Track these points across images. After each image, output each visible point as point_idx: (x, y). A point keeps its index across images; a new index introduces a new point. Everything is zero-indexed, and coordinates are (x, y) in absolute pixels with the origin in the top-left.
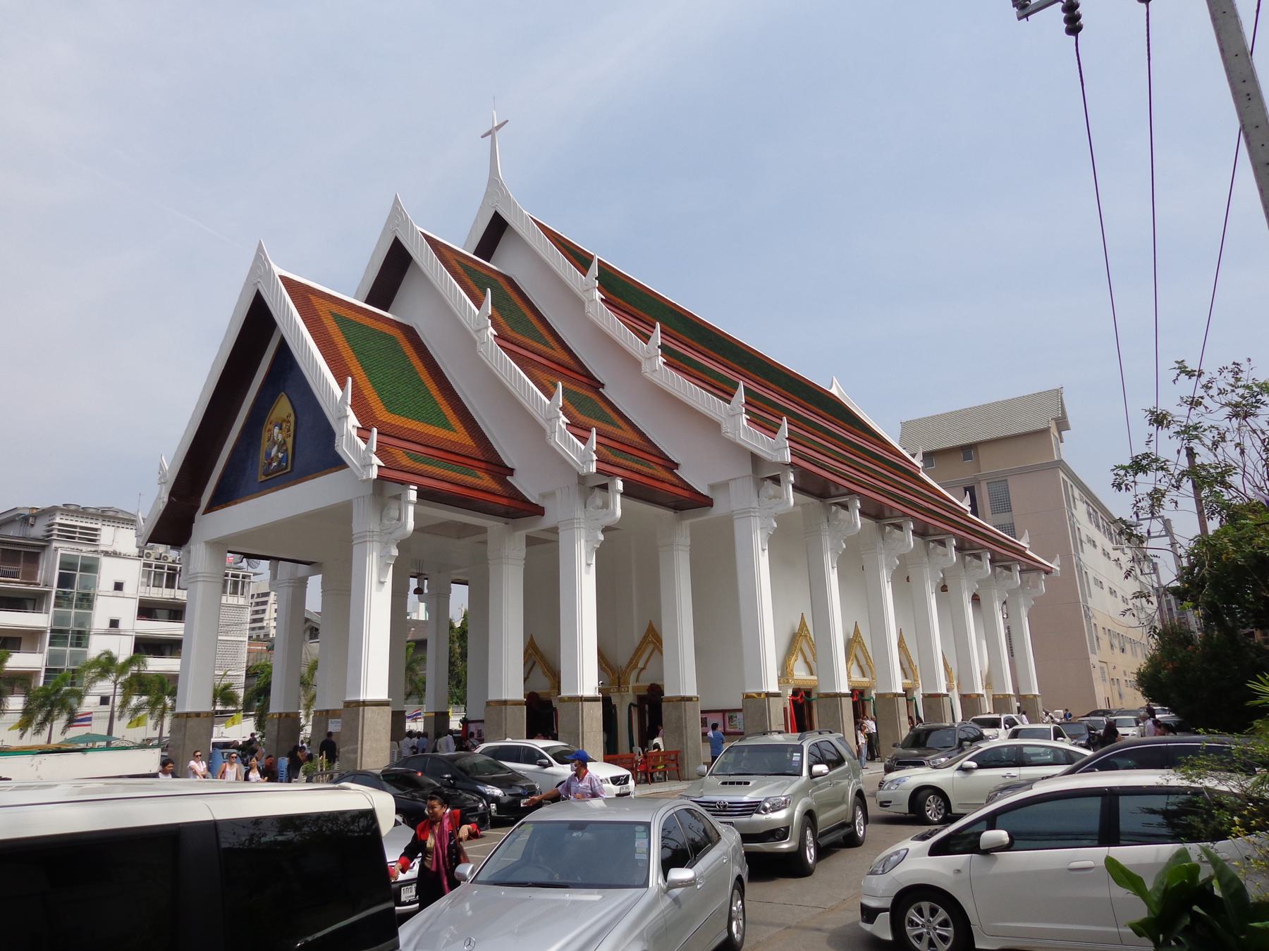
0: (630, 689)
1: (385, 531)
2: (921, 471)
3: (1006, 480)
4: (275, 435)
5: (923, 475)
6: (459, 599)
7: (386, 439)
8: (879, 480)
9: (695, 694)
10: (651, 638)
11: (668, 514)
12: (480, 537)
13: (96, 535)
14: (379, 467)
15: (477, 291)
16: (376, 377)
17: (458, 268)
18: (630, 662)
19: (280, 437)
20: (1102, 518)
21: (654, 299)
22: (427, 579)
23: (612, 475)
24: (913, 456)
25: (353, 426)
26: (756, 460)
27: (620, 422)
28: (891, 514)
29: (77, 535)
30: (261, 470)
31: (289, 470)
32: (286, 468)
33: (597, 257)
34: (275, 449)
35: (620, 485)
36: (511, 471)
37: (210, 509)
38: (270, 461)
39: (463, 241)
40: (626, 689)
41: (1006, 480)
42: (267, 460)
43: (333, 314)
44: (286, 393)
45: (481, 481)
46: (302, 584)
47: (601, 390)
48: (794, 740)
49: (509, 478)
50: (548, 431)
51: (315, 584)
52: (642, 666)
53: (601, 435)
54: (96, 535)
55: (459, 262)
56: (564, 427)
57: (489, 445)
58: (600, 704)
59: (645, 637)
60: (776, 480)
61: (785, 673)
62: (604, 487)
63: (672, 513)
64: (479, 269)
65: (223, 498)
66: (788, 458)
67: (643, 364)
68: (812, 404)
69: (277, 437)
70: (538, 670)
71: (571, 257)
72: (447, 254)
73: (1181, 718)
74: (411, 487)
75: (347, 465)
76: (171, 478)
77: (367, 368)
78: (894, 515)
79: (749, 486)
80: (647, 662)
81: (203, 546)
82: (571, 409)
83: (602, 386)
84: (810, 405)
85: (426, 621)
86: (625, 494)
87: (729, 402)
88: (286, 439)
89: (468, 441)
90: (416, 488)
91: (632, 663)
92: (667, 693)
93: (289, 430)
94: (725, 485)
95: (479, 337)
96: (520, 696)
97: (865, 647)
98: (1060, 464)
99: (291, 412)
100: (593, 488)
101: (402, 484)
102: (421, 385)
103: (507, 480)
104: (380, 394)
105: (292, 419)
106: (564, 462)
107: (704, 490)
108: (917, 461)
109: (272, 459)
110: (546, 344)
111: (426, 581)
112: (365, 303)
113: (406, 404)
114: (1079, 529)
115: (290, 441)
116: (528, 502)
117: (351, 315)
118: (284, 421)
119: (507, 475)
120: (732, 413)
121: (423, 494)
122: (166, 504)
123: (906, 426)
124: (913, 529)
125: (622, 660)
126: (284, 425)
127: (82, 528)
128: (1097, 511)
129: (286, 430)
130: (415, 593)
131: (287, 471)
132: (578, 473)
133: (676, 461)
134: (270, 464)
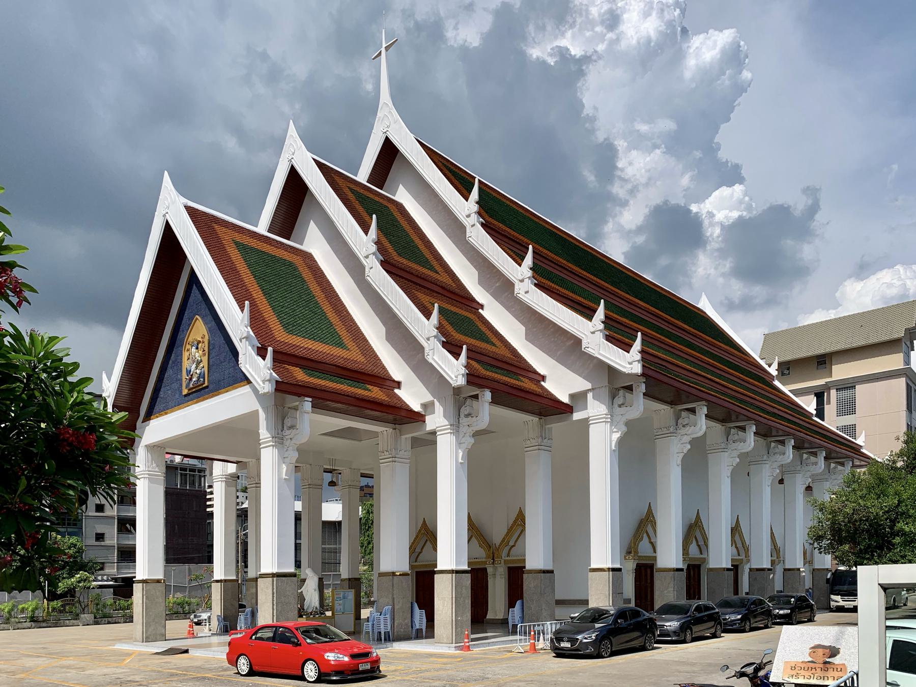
0: (502, 562)
5: (777, 383)
15: (364, 215)
16: (276, 300)
17: (351, 196)
21: (536, 223)
24: (770, 366)
26: (612, 372)
27: (498, 343)
33: (477, 178)
34: (194, 366)
42: (188, 376)
43: (236, 243)
45: (370, 392)
50: (427, 350)
52: (513, 544)
53: (472, 351)
55: (351, 189)
57: (378, 361)
58: (469, 575)
60: (629, 388)
64: (371, 196)
67: (516, 287)
68: (678, 320)
71: (456, 182)
72: (340, 182)
73: (701, 296)
74: (307, 399)
77: (267, 293)
82: (449, 328)
84: (677, 322)
85: (343, 504)
90: (310, 399)
91: (505, 541)
95: (367, 263)
96: (405, 567)
100: (466, 399)
103: (395, 394)
104: (279, 317)
107: (565, 399)
108: (773, 371)
110: (432, 268)
117: (253, 243)
124: (793, 444)
131: (204, 386)
134: (191, 379)
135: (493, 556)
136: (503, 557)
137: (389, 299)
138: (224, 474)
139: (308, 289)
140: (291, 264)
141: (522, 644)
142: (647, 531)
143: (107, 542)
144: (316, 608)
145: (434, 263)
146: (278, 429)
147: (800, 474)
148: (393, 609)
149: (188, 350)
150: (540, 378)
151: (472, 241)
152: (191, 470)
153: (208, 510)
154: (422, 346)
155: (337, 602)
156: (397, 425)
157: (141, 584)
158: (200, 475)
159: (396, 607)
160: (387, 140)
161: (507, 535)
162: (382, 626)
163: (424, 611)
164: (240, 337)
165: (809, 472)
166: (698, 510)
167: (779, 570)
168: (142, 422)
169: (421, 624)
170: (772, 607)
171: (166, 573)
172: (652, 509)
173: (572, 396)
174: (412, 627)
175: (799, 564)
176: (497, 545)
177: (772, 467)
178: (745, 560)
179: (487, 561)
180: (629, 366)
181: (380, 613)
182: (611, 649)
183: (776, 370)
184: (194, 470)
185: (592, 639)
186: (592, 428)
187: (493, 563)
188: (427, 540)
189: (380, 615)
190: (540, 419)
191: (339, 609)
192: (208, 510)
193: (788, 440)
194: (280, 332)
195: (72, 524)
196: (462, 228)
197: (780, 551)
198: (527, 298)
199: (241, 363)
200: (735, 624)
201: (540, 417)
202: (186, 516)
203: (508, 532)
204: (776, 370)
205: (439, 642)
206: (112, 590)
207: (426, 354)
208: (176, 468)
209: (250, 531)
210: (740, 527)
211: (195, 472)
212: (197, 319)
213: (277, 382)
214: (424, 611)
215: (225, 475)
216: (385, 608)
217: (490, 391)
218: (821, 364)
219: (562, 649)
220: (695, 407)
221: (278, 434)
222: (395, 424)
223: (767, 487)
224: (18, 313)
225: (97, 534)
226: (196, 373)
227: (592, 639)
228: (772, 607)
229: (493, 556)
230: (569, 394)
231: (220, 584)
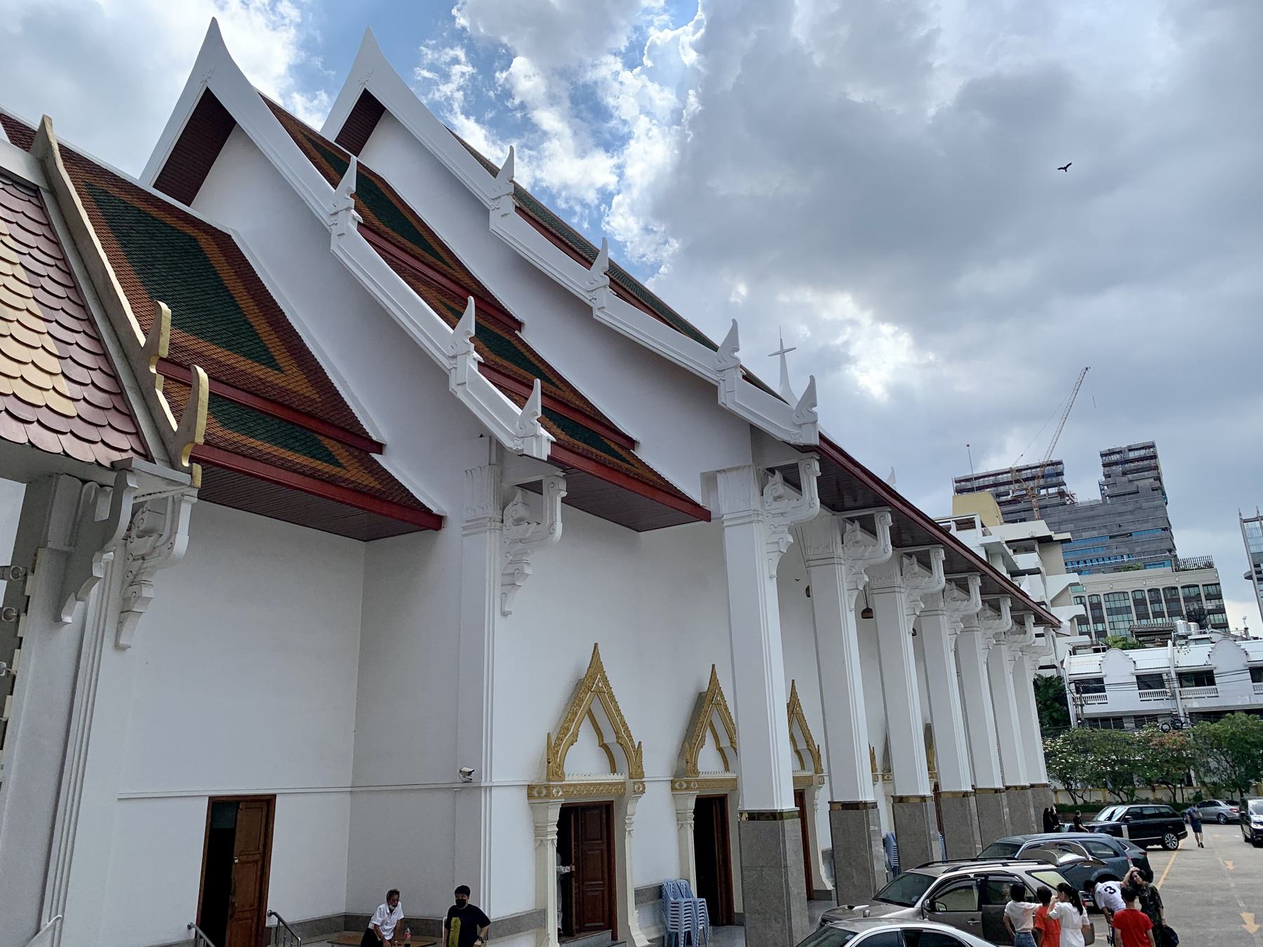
142: (711, 721)
147: (980, 633)
157: (835, 801)
160: (207, 89)
165: (990, 630)
166: (713, 666)
175: (868, 791)
177: (912, 598)
178: (816, 778)
180: (795, 431)
193: (972, 577)
197: (819, 756)
210: (800, 706)
220: (873, 514)
223: (848, 612)
230: (701, 474)
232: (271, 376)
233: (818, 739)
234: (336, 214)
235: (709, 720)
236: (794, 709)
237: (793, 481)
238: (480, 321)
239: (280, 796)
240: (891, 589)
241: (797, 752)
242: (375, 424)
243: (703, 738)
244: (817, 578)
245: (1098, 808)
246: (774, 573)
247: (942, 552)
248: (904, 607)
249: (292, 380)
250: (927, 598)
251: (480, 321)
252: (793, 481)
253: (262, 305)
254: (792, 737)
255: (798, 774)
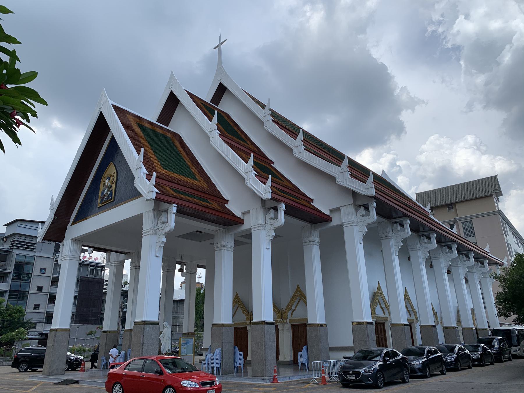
0: (288, 321)
1: (159, 229)
2: (430, 214)
3: (472, 221)
4: (106, 183)
5: (431, 216)
6: (201, 274)
7: (160, 181)
8: (417, 212)
9: (325, 323)
10: (298, 294)
11: (308, 225)
12: (211, 241)
13: (34, 246)
14: (157, 193)
18: (288, 306)
19: (109, 184)
20: (519, 241)
22: (185, 265)
23: (279, 201)
25: (144, 173)
26: (355, 194)
28: (424, 229)
29: (26, 244)
30: (99, 201)
31: (112, 200)
32: (111, 199)
35: (283, 206)
36: (227, 202)
37: (74, 223)
38: (103, 196)
39: (207, 97)
40: (286, 321)
41: (472, 221)
42: (102, 196)
43: (138, 124)
44: (113, 162)
46: (122, 263)
47: (272, 165)
48: (302, 361)
49: (226, 205)
50: (246, 179)
51: (128, 263)
54: (34, 246)
55: (202, 104)
56: (254, 176)
59: (295, 293)
61: (373, 312)
62: (275, 209)
63: (310, 225)
65: (82, 216)
66: (373, 192)
67: (294, 150)
69: (108, 183)
70: (240, 310)
72: (197, 100)
74: (174, 205)
75: (141, 194)
76: (56, 207)
78: (425, 230)
79: (352, 208)
80: (296, 306)
81: (70, 241)
83: (273, 163)
86: (286, 213)
87: (340, 167)
88: (112, 185)
89: (205, 186)
90: (176, 205)
91: (289, 307)
92: (310, 322)
93: (113, 181)
94: (338, 209)
97: (411, 301)
98: (500, 213)
99: (115, 171)
101: (169, 203)
102: (182, 159)
105: (115, 175)
106: (255, 195)
107: (327, 212)
108: (428, 209)
109: (104, 195)
110: (246, 142)
111: (185, 266)
112: (157, 122)
113: (173, 166)
114: (511, 245)
115: (114, 186)
116: (236, 216)
118: (111, 176)
119: (225, 204)
120: (342, 171)
121: (180, 212)
122: (52, 220)
123: (418, 195)
125: (284, 305)
126: (111, 178)
127: (27, 243)
128: (517, 237)
129: (112, 181)
130: (179, 271)
132: (262, 199)
133: (311, 198)
134: (103, 198)
135: (282, 317)
136: (288, 318)
137: (223, 153)
138: (116, 261)
139: (176, 149)
140: (167, 137)
141: (336, 376)
143: (41, 310)
144: (169, 350)
145: (247, 140)
146: (154, 224)
148: (222, 351)
149: (104, 181)
150: (310, 201)
151: (267, 128)
152: (97, 266)
153: (104, 291)
154: (243, 177)
155: (183, 346)
156: (226, 226)
158: (102, 270)
159: (224, 350)
160: (171, 91)
161: (290, 302)
162: (215, 364)
163: (242, 352)
164: (136, 168)
167: (459, 328)
168: (71, 226)
169: (240, 363)
170: (469, 353)
171: (71, 326)
172: (380, 285)
173: (331, 211)
174: (234, 365)
176: (284, 310)
179: (278, 320)
181: (212, 354)
182: (384, 381)
183: (430, 210)
184: (98, 267)
185: (371, 372)
186: (345, 229)
187: (282, 322)
188: (238, 306)
189: (213, 355)
190: (311, 225)
191: (183, 352)
192: (104, 291)
194: (160, 168)
195: (21, 298)
196: (262, 123)
198: (301, 156)
199: (135, 183)
200: (451, 365)
201: (312, 224)
202: (91, 295)
203: (291, 301)
204: (430, 210)
205: (254, 375)
206: (37, 341)
207: (246, 182)
208: (88, 265)
209: (129, 303)
211: (99, 268)
212: (111, 163)
213: (157, 193)
214: (242, 352)
215: (117, 262)
216: (216, 350)
217: (284, 204)
218: (450, 209)
219: (349, 380)
221: (154, 227)
222: (225, 226)
224: (4, 153)
225: (35, 305)
226: (107, 194)
227: (371, 372)
228: (469, 353)
229: (282, 317)
231: (106, 334)
232: (196, 182)
233: (415, 308)
234: (211, 131)
235: (378, 300)
236: (406, 296)
237: (367, 208)
238: (256, 160)
239: (144, 237)
240: (457, 266)
241: (409, 311)
242: (225, 194)
243: (377, 304)
244: (412, 254)
245: (14, 112)
246: (424, 264)
247: (435, 235)
248: (393, 245)
249: (201, 183)
250: (468, 268)
251: (256, 160)
252: (367, 208)
253: (194, 164)
254: (406, 306)
255: (409, 318)
